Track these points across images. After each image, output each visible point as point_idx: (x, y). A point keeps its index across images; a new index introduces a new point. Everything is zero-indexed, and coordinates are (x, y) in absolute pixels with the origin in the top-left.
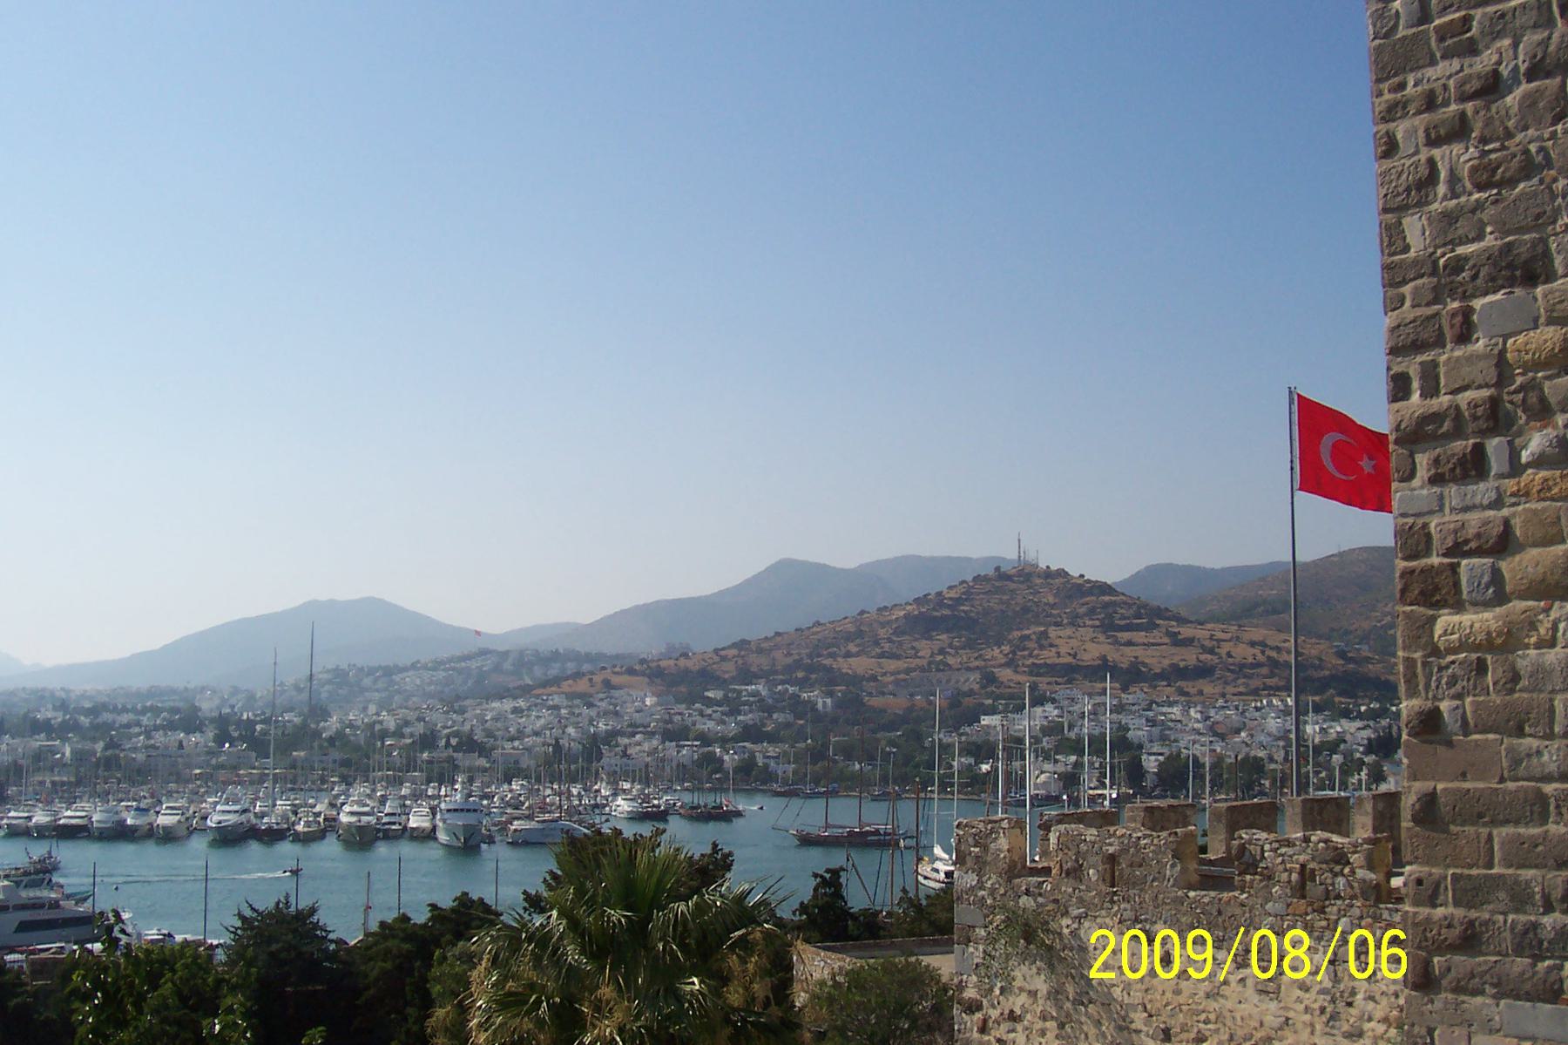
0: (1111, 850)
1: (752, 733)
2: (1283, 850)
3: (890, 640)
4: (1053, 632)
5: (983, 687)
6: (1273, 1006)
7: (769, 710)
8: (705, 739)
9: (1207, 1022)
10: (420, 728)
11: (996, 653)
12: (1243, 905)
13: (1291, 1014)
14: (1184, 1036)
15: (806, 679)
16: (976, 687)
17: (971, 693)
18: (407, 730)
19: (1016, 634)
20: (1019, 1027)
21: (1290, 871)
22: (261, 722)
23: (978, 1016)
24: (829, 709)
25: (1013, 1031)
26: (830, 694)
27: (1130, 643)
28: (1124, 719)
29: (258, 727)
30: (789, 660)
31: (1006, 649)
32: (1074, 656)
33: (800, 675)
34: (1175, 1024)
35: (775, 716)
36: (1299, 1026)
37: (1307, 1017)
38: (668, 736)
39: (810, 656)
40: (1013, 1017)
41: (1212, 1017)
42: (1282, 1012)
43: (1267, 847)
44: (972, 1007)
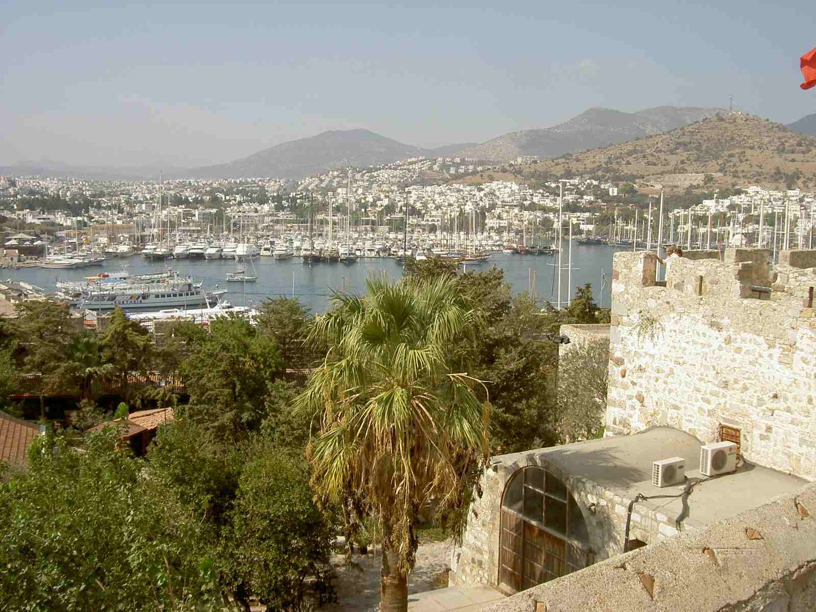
0: (701, 273)
1: (572, 208)
2: (799, 278)
3: (653, 155)
4: (749, 152)
5: (705, 184)
6: (788, 372)
7: (581, 194)
8: (544, 209)
9: (749, 379)
10: (386, 202)
11: (713, 165)
12: (775, 310)
13: (797, 377)
14: (736, 386)
15: (604, 176)
16: (702, 183)
17: (698, 186)
18: (379, 203)
19: (726, 153)
20: (644, 375)
21: (804, 291)
22: (300, 198)
23: (621, 368)
24: (615, 194)
25: (641, 377)
26: (617, 186)
27: (793, 160)
28: (330, 225)
29: (298, 201)
30: (595, 165)
31: (720, 162)
32: (760, 167)
33: (600, 173)
34: (731, 379)
35: (585, 197)
36: (802, 385)
37: (807, 380)
38: (522, 207)
39: (606, 163)
40: (641, 369)
41: (752, 376)
42: (792, 376)
43: (791, 276)
44: (619, 362)
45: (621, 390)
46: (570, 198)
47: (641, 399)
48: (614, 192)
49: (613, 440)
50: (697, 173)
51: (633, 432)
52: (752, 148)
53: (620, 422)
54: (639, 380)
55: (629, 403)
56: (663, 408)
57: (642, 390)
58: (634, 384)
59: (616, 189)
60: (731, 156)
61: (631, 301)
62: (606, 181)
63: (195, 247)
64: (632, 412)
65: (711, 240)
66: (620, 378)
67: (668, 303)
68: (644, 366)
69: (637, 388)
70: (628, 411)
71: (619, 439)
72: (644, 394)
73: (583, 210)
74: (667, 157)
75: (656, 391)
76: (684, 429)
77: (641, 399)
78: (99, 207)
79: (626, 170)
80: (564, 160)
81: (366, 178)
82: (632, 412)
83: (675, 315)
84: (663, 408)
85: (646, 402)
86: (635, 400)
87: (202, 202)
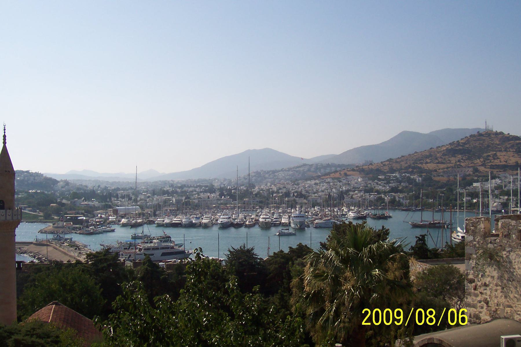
1: (394, 190)
3: (441, 158)
4: (498, 154)
5: (474, 173)
7: (400, 182)
8: (379, 192)
10: (284, 190)
16: (471, 173)
17: (469, 175)
18: (280, 191)
19: (485, 155)
20: (488, 288)
22: (234, 189)
23: (473, 284)
24: (420, 182)
25: (486, 290)
26: (421, 176)
29: (233, 191)
30: (407, 165)
31: (482, 160)
32: (506, 162)
38: (366, 191)
39: (414, 163)
44: (471, 281)
45: (474, 298)
46: (393, 185)
47: (487, 303)
48: (419, 179)
49: (468, 328)
50: (469, 167)
51: (482, 322)
52: (500, 151)
53: (474, 316)
54: (485, 291)
55: (479, 304)
56: (501, 307)
57: (487, 297)
58: (481, 293)
59: (420, 179)
60: (489, 156)
61: (477, 246)
62: (414, 174)
63: (175, 220)
64: (481, 310)
65: (483, 208)
66: (473, 291)
67: (501, 246)
68: (487, 283)
69: (484, 296)
70: (479, 309)
71: (473, 327)
72: (488, 299)
73: (401, 191)
74: (450, 159)
75: (496, 297)
76: (516, 319)
77: (487, 303)
78: (117, 196)
79: (425, 167)
80: (388, 163)
81: (271, 176)
82: (481, 310)
83: (506, 253)
84: (501, 307)
85: (490, 304)
86: (482, 303)
87: (176, 192)
